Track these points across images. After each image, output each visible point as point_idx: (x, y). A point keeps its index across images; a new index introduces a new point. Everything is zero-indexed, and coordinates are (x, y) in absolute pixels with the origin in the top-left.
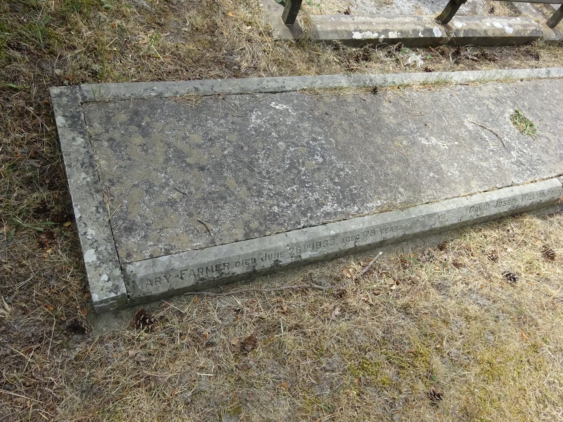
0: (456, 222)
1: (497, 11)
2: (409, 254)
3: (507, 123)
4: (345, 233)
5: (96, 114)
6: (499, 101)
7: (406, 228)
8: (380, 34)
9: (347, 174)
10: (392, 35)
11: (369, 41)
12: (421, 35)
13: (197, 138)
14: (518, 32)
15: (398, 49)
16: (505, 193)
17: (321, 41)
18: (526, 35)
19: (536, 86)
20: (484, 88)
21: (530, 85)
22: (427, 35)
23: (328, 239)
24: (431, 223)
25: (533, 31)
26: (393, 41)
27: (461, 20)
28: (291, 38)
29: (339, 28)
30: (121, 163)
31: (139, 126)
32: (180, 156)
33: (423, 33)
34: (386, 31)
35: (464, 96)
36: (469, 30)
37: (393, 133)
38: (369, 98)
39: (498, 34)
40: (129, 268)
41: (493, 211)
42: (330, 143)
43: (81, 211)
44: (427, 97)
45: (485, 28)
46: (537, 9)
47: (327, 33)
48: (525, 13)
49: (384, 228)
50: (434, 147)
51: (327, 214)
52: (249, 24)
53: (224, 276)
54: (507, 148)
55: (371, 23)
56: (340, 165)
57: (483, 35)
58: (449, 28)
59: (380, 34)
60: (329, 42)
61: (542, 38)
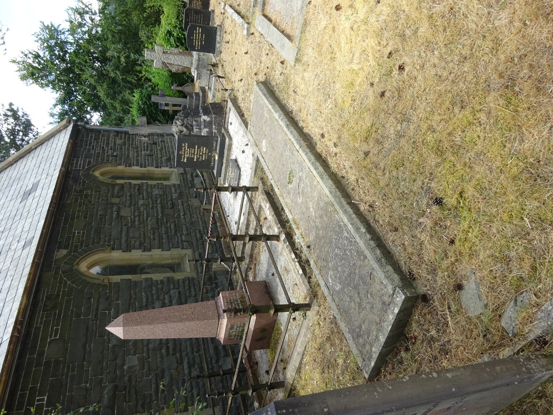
0: (330, 180)
1: (265, 216)
2: (349, 190)
3: (294, 184)
4: (349, 221)
5: (364, 351)
6: (289, 193)
7: (339, 199)
8: (295, 262)
9: (335, 235)
10: (293, 256)
11: (300, 265)
12: (288, 243)
13: (353, 304)
14: (266, 201)
15: (297, 249)
16: (312, 169)
17: (310, 286)
18: (266, 197)
19: (278, 181)
20: (288, 202)
21: (278, 184)
22: (286, 240)
23: (354, 226)
24: (334, 190)
25: (263, 195)
26: (296, 254)
27: (274, 230)
28: (315, 301)
29: (302, 282)
30: (371, 325)
31: (360, 331)
32: (360, 305)
33: (286, 243)
34: (293, 260)
35: (294, 209)
36: (276, 224)
37: (317, 228)
38: (312, 247)
39: (271, 210)
40: (392, 293)
41: (321, 169)
42: (330, 250)
43: (388, 327)
44: (301, 223)
45: (272, 217)
46: (255, 199)
47: (306, 286)
48: (259, 204)
49: (342, 207)
50: (313, 208)
51: (348, 233)
52: (319, 324)
53: (382, 256)
54: (300, 178)
55: (294, 269)
56: (334, 240)
57: (275, 216)
58: (279, 233)
59: (295, 262)
60: (309, 282)
61: (264, 189)
